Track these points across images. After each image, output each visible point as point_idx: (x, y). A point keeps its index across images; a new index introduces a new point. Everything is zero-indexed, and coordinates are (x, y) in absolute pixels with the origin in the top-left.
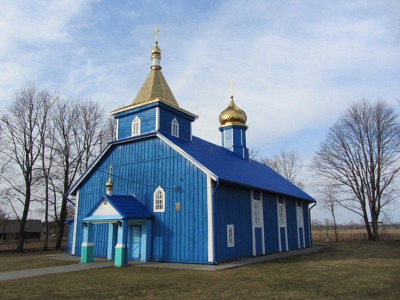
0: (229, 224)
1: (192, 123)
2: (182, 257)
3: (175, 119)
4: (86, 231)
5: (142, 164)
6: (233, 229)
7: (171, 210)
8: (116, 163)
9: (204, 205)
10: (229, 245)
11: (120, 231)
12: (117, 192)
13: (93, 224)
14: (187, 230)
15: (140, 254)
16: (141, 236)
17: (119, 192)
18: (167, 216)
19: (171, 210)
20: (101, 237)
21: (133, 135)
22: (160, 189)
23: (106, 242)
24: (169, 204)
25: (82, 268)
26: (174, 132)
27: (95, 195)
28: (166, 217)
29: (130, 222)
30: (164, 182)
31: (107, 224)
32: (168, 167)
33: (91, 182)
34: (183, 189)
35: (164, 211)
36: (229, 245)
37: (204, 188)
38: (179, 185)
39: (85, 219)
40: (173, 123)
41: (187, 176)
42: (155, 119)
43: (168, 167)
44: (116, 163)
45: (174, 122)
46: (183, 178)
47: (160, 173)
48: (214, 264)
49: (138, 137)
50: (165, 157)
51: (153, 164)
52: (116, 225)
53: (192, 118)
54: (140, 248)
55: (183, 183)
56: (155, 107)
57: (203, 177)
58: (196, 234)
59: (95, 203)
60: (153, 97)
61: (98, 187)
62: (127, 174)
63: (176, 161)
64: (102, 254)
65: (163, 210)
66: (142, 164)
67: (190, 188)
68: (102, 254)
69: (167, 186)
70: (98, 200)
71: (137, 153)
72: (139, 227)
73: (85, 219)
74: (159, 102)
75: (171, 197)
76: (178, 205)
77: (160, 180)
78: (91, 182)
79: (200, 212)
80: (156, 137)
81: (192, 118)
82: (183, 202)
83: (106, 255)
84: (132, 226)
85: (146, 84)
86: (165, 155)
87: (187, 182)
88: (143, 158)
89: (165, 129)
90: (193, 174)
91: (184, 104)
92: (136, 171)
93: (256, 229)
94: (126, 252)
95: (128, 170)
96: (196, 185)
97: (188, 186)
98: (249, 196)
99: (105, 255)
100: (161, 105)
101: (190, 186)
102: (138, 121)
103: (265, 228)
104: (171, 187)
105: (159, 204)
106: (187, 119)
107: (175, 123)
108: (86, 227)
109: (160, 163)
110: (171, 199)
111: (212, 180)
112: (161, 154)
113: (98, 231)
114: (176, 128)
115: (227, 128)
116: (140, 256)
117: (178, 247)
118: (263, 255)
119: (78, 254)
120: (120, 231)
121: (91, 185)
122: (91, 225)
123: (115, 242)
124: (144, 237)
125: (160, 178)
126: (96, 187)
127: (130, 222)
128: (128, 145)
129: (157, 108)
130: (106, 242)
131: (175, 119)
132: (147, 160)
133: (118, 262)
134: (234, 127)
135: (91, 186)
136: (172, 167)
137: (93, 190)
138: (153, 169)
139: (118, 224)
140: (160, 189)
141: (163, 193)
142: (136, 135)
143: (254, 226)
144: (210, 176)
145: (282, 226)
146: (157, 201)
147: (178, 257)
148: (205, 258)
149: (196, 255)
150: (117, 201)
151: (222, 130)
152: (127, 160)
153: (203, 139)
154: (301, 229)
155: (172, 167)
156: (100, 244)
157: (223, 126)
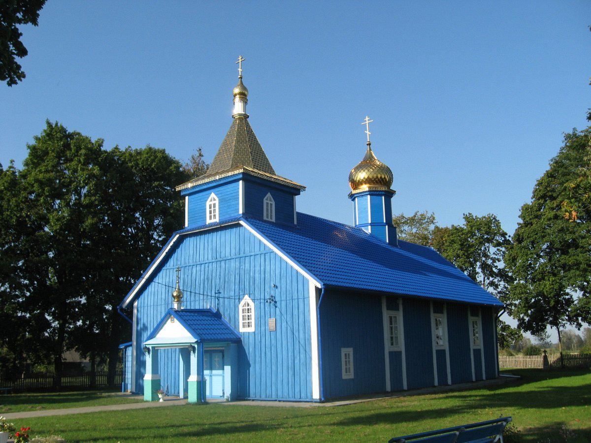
0: (344, 347)
1: (297, 197)
2: (280, 394)
3: (269, 195)
4: (148, 359)
5: (223, 263)
6: (351, 354)
7: (263, 328)
8: (187, 261)
9: (306, 323)
10: (345, 376)
11: (194, 359)
12: (188, 303)
13: (157, 350)
14: (285, 357)
15: (223, 390)
16: (223, 369)
17: (192, 304)
18: (258, 337)
19: (263, 328)
20: (169, 368)
21: (208, 221)
22: (247, 299)
23: (177, 375)
24: (261, 320)
25: (146, 405)
26: (267, 215)
27: (159, 308)
28: (256, 338)
29: (209, 346)
30: (252, 289)
31: (170, 351)
32: (257, 268)
33: (153, 289)
34: (277, 299)
35: (254, 331)
36: (345, 376)
37: (306, 298)
38: (273, 293)
39: (147, 343)
40: (265, 201)
41: (283, 280)
42: (238, 198)
43: (257, 268)
44: (187, 261)
45: (267, 199)
46: (278, 285)
47: (247, 276)
48: (321, 401)
49: (215, 224)
50: (253, 254)
51: (237, 263)
52: (186, 351)
53: (296, 190)
54: (220, 384)
55: (278, 291)
56: (237, 180)
57: (305, 282)
58: (297, 361)
59: (159, 320)
60: (235, 167)
61: (163, 296)
62: (202, 277)
63: (268, 260)
64: (173, 391)
65: (252, 329)
66: (223, 263)
67: (288, 299)
68: (173, 391)
69: (257, 296)
70: (163, 315)
71: (214, 248)
72: (221, 354)
73: (147, 343)
74: (243, 173)
75: (263, 311)
76: (271, 322)
77: (247, 287)
78: (153, 289)
79: (301, 332)
80: (239, 225)
81: (296, 190)
82: (278, 318)
83: (179, 393)
84: (210, 353)
85: (225, 144)
86: (253, 251)
87: (284, 289)
88: (223, 255)
89: (253, 213)
90: (291, 278)
91: (284, 170)
92: (214, 275)
93: (391, 353)
94: (201, 385)
95: (202, 273)
96: (296, 293)
97: (285, 296)
98: (381, 309)
99: (176, 392)
100: (247, 178)
101: (288, 296)
102: (215, 200)
103: (406, 351)
104: (262, 297)
105: (247, 321)
106: (287, 193)
107: (269, 202)
108: (149, 353)
109: (246, 262)
110: (263, 314)
111: (317, 288)
112: (247, 249)
113: (166, 359)
114: (271, 207)
115: (362, 195)
116: (224, 393)
117: (274, 379)
118: (405, 391)
119: (139, 390)
120: (194, 359)
121: (153, 294)
122: (155, 351)
123: (187, 373)
124: (228, 369)
125: (247, 283)
126: (159, 297)
127: (207, 346)
128: (202, 237)
129: (241, 182)
130: (177, 375)
131: (269, 195)
132: (230, 258)
133: (193, 397)
134: (372, 193)
135: (153, 296)
136: (262, 268)
137: (156, 300)
138: (237, 271)
139: (190, 349)
140: (247, 299)
141: (252, 305)
142: (213, 221)
143: (472, 347)
144: (313, 284)
145: (476, 348)
146: (243, 316)
147: (273, 394)
148: (309, 395)
149: (297, 390)
150: (188, 317)
151: (352, 197)
152: (201, 257)
153: (151, 362)
154: (477, 352)
155: (262, 268)
156: (170, 377)
157: (354, 192)
